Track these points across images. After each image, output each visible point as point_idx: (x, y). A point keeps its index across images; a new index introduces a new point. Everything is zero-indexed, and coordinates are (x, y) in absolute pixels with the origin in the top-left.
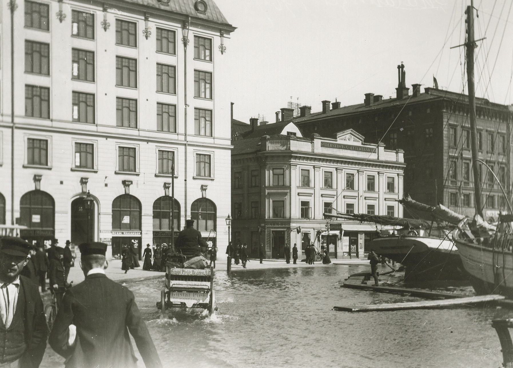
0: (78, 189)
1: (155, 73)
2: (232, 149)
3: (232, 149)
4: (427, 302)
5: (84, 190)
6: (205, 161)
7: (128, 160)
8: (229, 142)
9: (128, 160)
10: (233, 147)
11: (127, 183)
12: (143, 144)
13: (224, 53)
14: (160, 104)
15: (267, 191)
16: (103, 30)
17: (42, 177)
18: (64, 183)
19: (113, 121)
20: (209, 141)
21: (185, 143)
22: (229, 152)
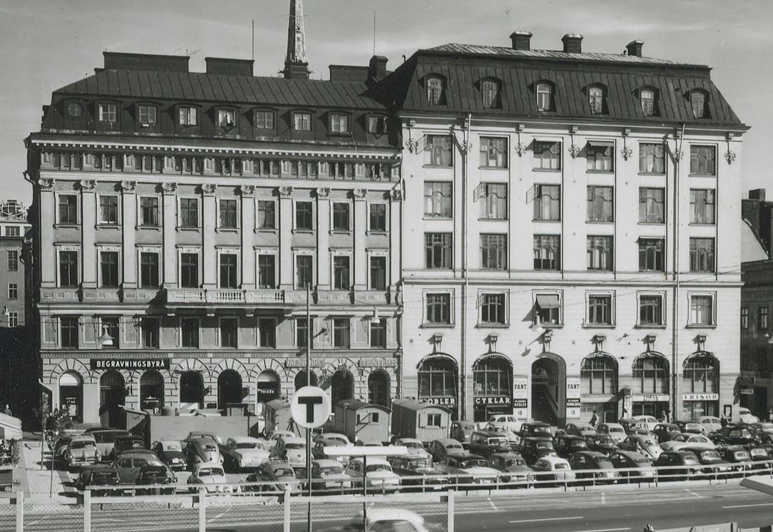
0: (537, 350)
1: (586, 197)
2: (742, 287)
3: (742, 287)
4: (230, 527)
5: (702, 349)
6: (707, 305)
7: (601, 311)
8: (738, 278)
9: (601, 311)
10: (743, 284)
11: (599, 339)
12: (620, 290)
13: (732, 162)
14: (538, 237)
15: (546, 339)
16: (518, 155)
17: (656, 338)
18: (518, 343)
19: (635, 265)
20: (709, 278)
21: (464, 281)
22: (739, 290)
